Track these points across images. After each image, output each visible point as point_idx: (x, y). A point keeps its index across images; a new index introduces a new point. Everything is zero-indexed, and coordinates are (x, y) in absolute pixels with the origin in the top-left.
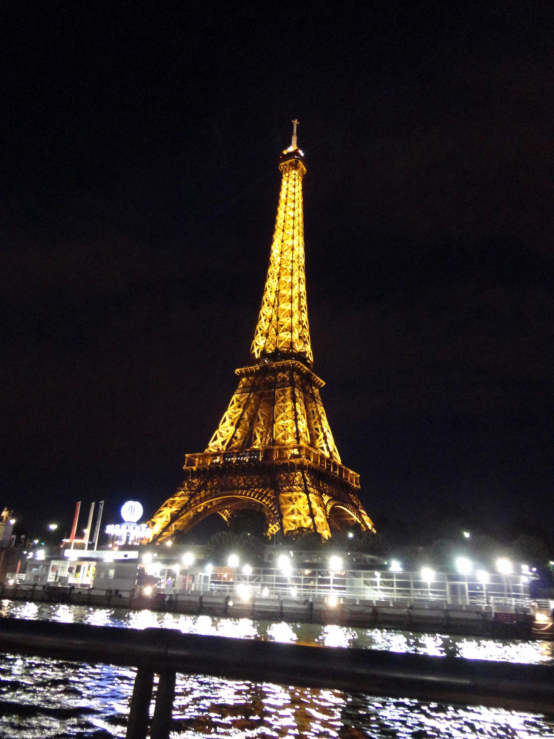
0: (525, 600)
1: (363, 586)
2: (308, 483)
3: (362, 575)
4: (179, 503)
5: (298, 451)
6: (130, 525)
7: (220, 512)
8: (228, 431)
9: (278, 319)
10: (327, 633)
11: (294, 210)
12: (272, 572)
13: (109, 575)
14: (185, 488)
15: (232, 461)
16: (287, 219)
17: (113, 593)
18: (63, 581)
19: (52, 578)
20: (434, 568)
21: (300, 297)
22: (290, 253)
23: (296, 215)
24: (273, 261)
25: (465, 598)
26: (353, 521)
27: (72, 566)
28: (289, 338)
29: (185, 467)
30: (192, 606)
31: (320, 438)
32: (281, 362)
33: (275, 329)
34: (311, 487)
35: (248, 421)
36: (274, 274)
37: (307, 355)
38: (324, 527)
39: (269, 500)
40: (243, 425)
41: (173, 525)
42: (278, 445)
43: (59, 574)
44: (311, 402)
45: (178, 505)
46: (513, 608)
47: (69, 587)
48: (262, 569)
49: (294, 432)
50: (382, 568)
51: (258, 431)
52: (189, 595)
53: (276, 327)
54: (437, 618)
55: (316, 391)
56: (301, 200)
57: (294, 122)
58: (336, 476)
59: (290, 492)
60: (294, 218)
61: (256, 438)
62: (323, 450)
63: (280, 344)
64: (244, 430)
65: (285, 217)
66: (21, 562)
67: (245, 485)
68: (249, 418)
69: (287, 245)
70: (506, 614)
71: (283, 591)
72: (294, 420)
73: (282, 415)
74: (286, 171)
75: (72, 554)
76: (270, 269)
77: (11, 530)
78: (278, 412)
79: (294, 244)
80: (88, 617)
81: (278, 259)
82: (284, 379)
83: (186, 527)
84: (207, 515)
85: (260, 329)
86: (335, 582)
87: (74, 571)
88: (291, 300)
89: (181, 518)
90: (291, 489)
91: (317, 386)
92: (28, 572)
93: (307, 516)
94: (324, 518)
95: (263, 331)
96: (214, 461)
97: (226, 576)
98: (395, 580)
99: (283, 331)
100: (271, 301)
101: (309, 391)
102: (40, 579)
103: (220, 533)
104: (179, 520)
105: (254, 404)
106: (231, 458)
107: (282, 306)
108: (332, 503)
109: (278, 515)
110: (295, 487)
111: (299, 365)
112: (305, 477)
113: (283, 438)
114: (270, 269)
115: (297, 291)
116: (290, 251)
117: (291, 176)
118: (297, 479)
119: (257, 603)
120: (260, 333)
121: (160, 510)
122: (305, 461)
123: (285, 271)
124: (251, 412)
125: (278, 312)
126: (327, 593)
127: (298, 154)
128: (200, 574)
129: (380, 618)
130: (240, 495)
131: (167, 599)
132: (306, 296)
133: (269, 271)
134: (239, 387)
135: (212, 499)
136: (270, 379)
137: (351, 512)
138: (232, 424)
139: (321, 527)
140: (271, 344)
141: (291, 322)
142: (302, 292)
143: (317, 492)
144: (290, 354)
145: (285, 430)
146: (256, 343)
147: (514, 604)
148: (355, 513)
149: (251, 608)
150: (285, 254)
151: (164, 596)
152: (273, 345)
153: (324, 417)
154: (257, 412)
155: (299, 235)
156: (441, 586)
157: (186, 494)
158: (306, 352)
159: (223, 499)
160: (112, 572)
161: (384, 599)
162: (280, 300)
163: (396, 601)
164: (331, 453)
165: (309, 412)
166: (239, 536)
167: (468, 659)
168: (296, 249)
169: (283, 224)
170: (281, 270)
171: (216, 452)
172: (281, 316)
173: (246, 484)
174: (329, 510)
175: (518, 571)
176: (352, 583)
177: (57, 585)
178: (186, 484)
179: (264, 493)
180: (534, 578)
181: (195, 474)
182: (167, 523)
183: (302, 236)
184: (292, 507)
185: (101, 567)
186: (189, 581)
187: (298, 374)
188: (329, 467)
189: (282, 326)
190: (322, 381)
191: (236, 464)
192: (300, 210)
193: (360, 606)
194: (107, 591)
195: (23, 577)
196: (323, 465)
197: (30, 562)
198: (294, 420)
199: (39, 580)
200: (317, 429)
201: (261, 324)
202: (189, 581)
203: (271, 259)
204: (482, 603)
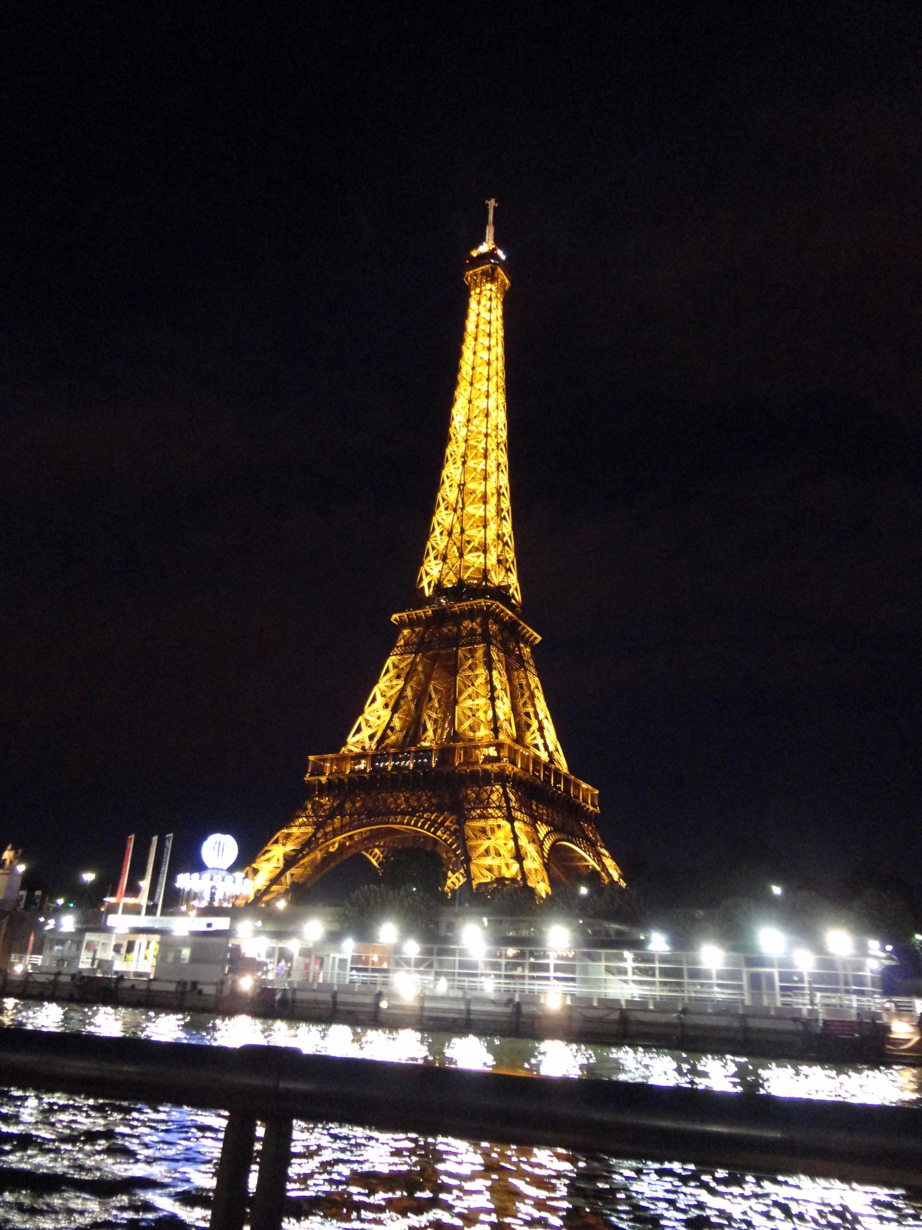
0: (874, 998)
1: (604, 976)
2: (513, 804)
3: (603, 957)
4: (297, 838)
5: (496, 750)
6: (217, 874)
7: (367, 852)
8: (379, 718)
9: (463, 531)
10: (544, 1054)
11: (489, 349)
12: (452, 952)
13: (182, 957)
14: (309, 813)
15: (385, 768)
16: (478, 364)
17: (189, 987)
18: (105, 968)
19: (87, 963)
20: (722, 945)
21: (499, 494)
22: (483, 421)
23: (493, 357)
24: (454, 435)
25: (774, 994)
26: (587, 866)
27: (120, 942)
28: (481, 563)
29: (307, 778)
30: (319, 1008)
31: (532, 729)
32: (468, 603)
33: (458, 548)
34: (517, 810)
35: (413, 700)
36: (457, 456)
37: (511, 591)
38: (539, 877)
39: (448, 833)
40: (404, 708)
41: (288, 874)
42: (463, 740)
43: (98, 956)
44: (517, 670)
45: (297, 841)
46: (854, 1012)
47: (115, 977)
48: (436, 947)
49: (489, 720)
50: (636, 945)
51: (430, 717)
52: (314, 991)
53: (459, 544)
54: (727, 1029)
55: (527, 651)
56: (501, 333)
57: (489, 203)
58: (559, 792)
59: (483, 818)
60: (489, 364)
61: (425, 730)
62: (538, 749)
63: (466, 573)
64: (407, 716)
65: (474, 361)
66: (35, 936)
67: (408, 808)
68: (414, 696)
69: (478, 407)
70: (842, 1022)
71: (472, 984)
72: (489, 699)
73: (470, 690)
74: (476, 285)
75: (120, 923)
76: (449, 447)
77: (18, 882)
78: (462, 686)
79: (489, 407)
80: (147, 1026)
81: (463, 432)
82: (472, 632)
83: (310, 877)
84: (345, 857)
85: (433, 548)
86: (558, 968)
87: (123, 950)
88: (484, 500)
89: (302, 862)
90: (484, 814)
91: (527, 642)
92: (47, 952)
93: (511, 858)
94: (539, 863)
95: (438, 550)
96: (357, 767)
97: (375, 958)
98: (657, 965)
99: (470, 551)
100: (451, 502)
101: (514, 651)
102: (66, 963)
103: (366, 887)
104: (297, 866)
105: (422, 672)
106: (385, 762)
107: (470, 509)
108: (553, 838)
109: (463, 858)
110: (490, 811)
111: (498, 607)
112: (508, 793)
113: (472, 728)
114: (449, 447)
115: (495, 485)
116: (483, 418)
117: (484, 293)
118: (494, 797)
119: (427, 1004)
120: (432, 554)
121: (266, 848)
122: (508, 768)
123: (475, 451)
124: (418, 686)
125: (462, 520)
126: (544, 988)
127: (496, 257)
128: (332, 955)
129: (633, 1028)
130: (399, 824)
131: (278, 997)
132: (509, 493)
133: (448, 451)
134: (398, 645)
135: (354, 830)
136: (450, 630)
137: (585, 851)
138: (386, 706)
139: (534, 878)
140: (451, 573)
141: (484, 536)
142: (503, 486)
143: (528, 819)
144: (482, 590)
145: (474, 715)
146: (425, 570)
147: (855, 1005)
148: (591, 854)
149: (418, 1012)
150: (474, 424)
151: (273, 991)
152: (455, 574)
153: (539, 694)
154: (428, 686)
155: (497, 391)
156: (734, 975)
157: (309, 822)
158: (509, 587)
159: (371, 830)
160: (186, 953)
161: (640, 997)
162: (465, 499)
163: (659, 1000)
164: (550, 755)
165: (514, 686)
166: (399, 893)
167: (778, 1097)
168: (493, 414)
169: (471, 372)
170: (468, 449)
171: (359, 753)
172: (468, 526)
173: (410, 806)
174: (548, 848)
175: (863, 950)
176: (585, 970)
177: (95, 973)
178: (310, 806)
179: (439, 821)
180: (888, 962)
181: (324, 790)
182: (278, 871)
183: (503, 393)
184: (486, 844)
185: (168, 944)
186: (314, 967)
187: (496, 622)
188: (547, 777)
189: (469, 542)
190: (536, 634)
191: (393, 773)
192: (499, 350)
193: (599, 1009)
194: (179, 983)
195: (39, 960)
196: (538, 774)
197: (50, 936)
198: (489, 699)
199: (65, 965)
200: (528, 714)
201: (435, 539)
202: (314, 967)
203: (452, 430)
204: (803, 1004)
